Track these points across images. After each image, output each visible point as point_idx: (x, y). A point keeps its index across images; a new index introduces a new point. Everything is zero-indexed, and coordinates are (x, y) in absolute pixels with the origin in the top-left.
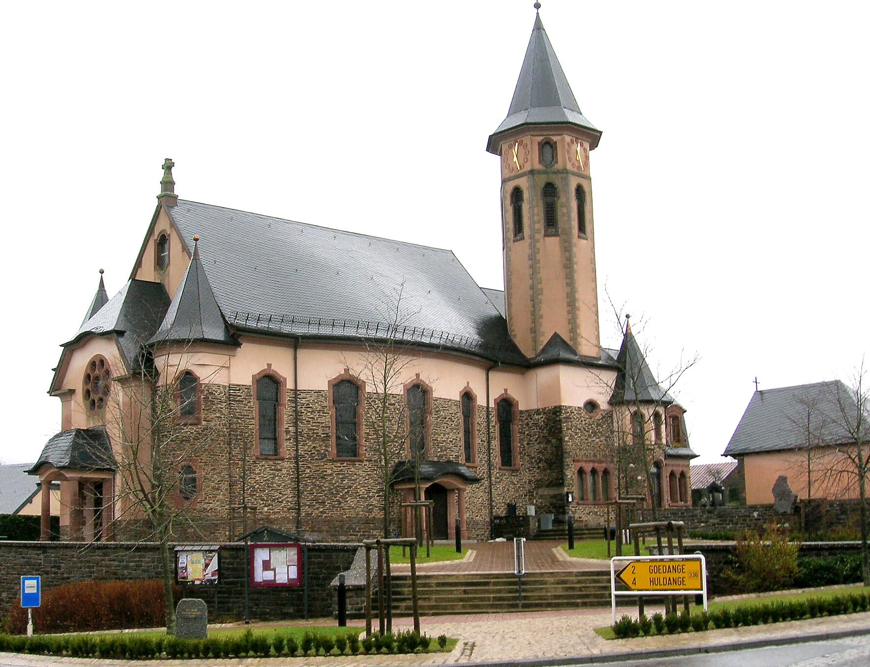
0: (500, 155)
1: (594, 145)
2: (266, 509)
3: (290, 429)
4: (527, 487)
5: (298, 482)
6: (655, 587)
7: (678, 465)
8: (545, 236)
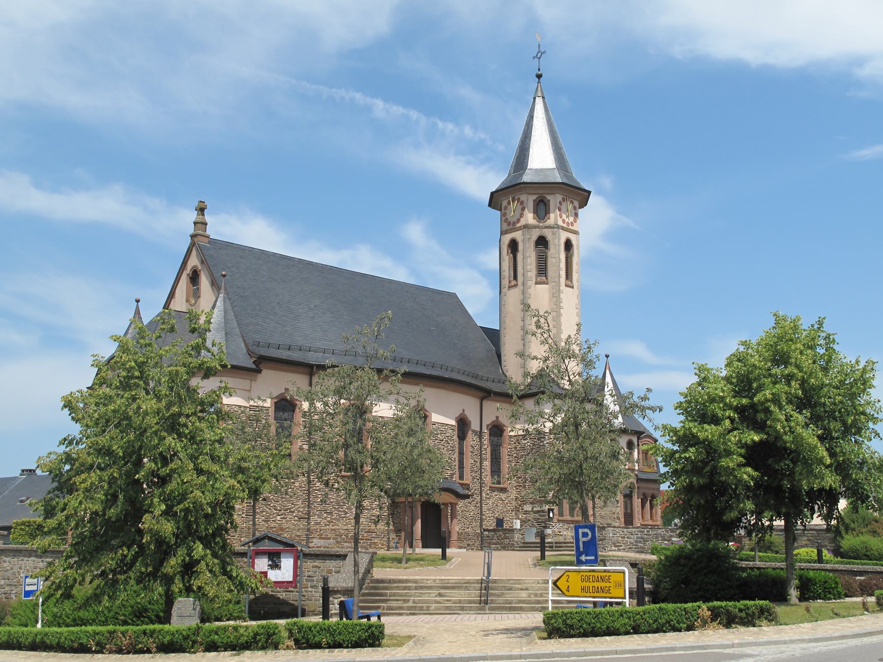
0: (500, 210)
1: (584, 203)
2: (279, 518)
3: (304, 446)
4: (514, 503)
5: (309, 494)
6: (585, 594)
7: (649, 488)
8: (537, 283)
